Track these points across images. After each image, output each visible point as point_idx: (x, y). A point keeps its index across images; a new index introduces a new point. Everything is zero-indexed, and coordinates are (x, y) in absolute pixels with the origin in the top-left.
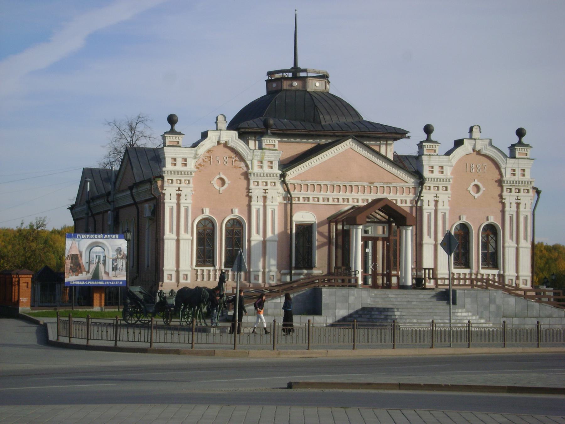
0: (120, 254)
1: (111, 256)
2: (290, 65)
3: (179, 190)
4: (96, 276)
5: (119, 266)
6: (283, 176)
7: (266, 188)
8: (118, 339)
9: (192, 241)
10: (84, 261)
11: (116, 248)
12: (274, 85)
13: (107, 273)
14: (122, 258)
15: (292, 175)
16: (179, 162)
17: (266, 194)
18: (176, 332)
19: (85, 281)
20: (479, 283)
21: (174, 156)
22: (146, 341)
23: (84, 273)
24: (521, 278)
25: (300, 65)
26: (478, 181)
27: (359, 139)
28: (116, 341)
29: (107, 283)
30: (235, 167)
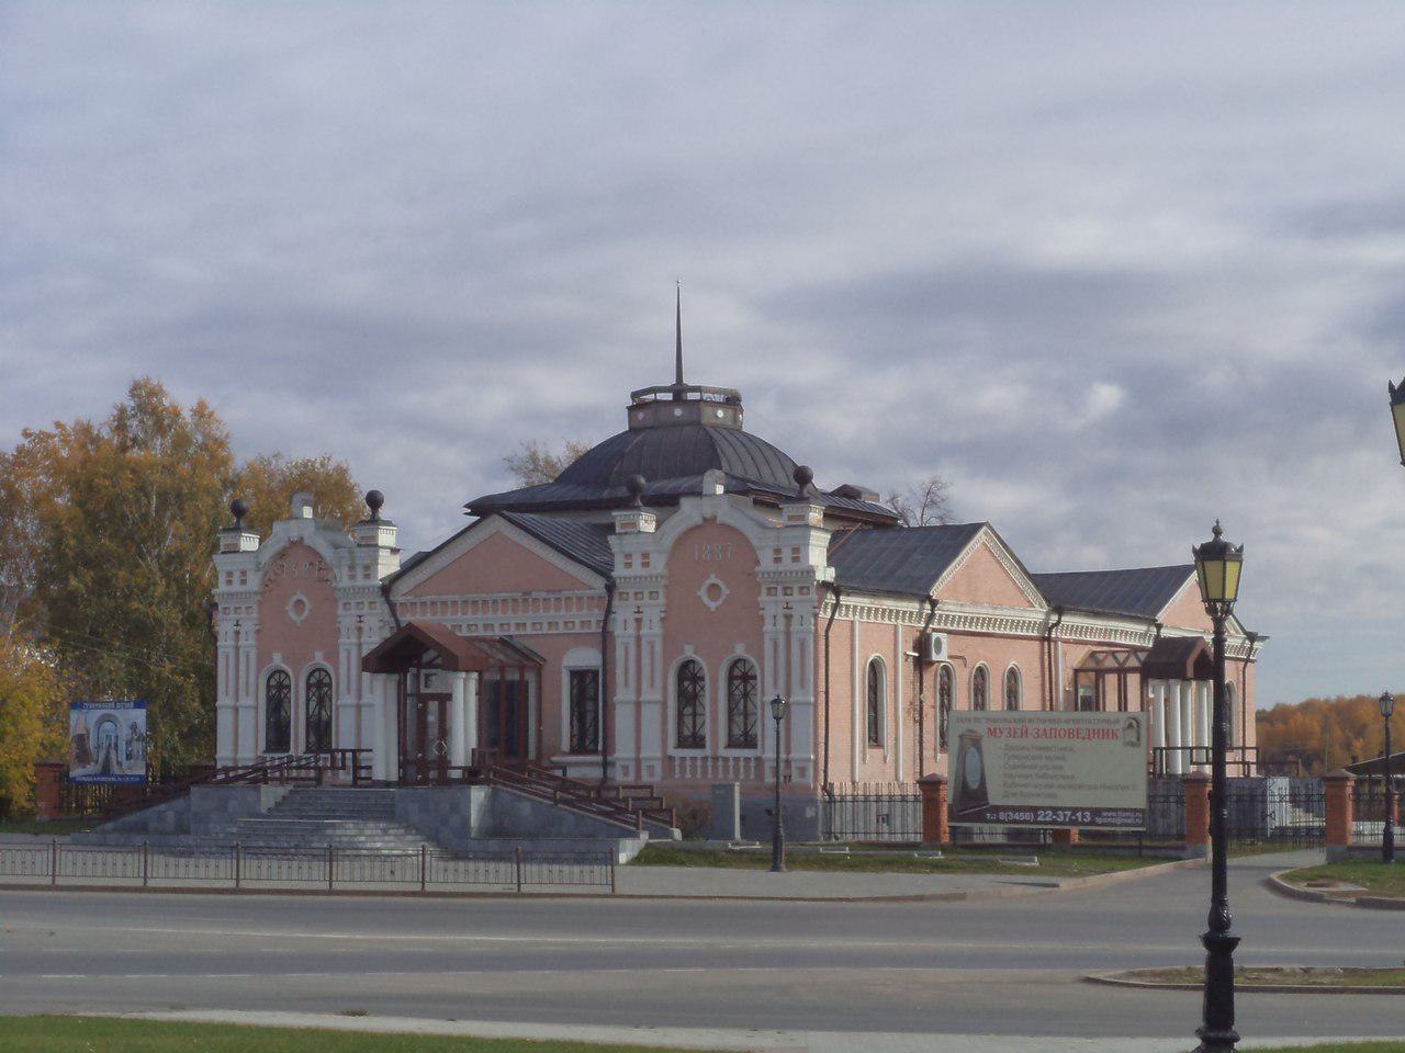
1: (124, 738)
2: (671, 380)
4: (106, 770)
7: (359, 613)
8: (149, 875)
9: (664, 704)
10: (92, 744)
12: (641, 416)
16: (236, 578)
17: (362, 625)
20: (277, 774)
21: (229, 568)
22: (509, 881)
24: (794, 765)
25: (688, 381)
26: (717, 577)
27: (514, 515)
28: (331, 881)
29: (120, 779)
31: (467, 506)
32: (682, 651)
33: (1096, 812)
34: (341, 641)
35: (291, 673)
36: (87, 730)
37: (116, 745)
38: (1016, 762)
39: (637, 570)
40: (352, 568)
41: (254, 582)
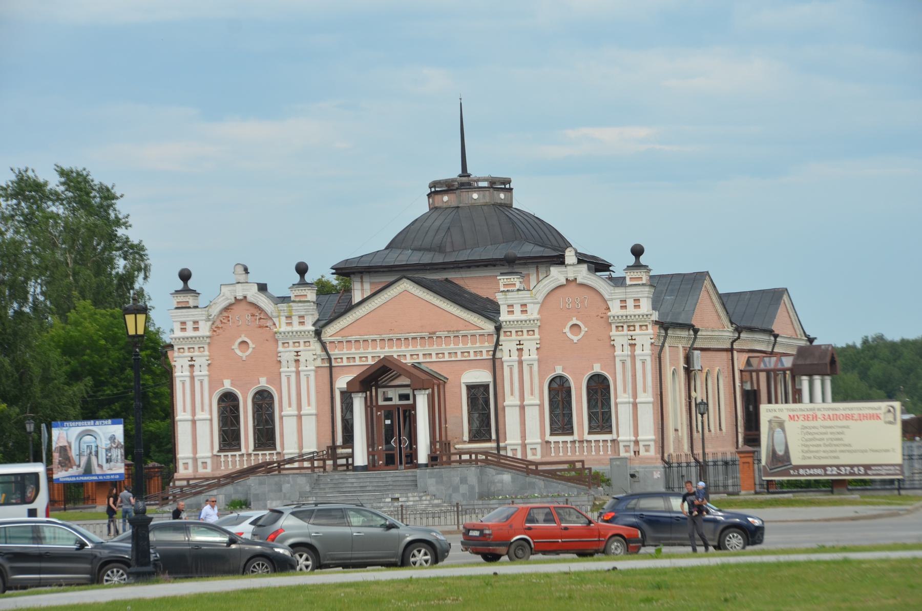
0: (114, 442)
1: (104, 446)
3: (192, 360)
4: (88, 471)
5: (114, 457)
6: (318, 333)
7: (297, 349)
10: (74, 453)
11: (109, 435)
13: (100, 466)
14: (117, 447)
15: (329, 333)
19: (75, 476)
23: (75, 467)
29: (101, 478)
30: (260, 327)
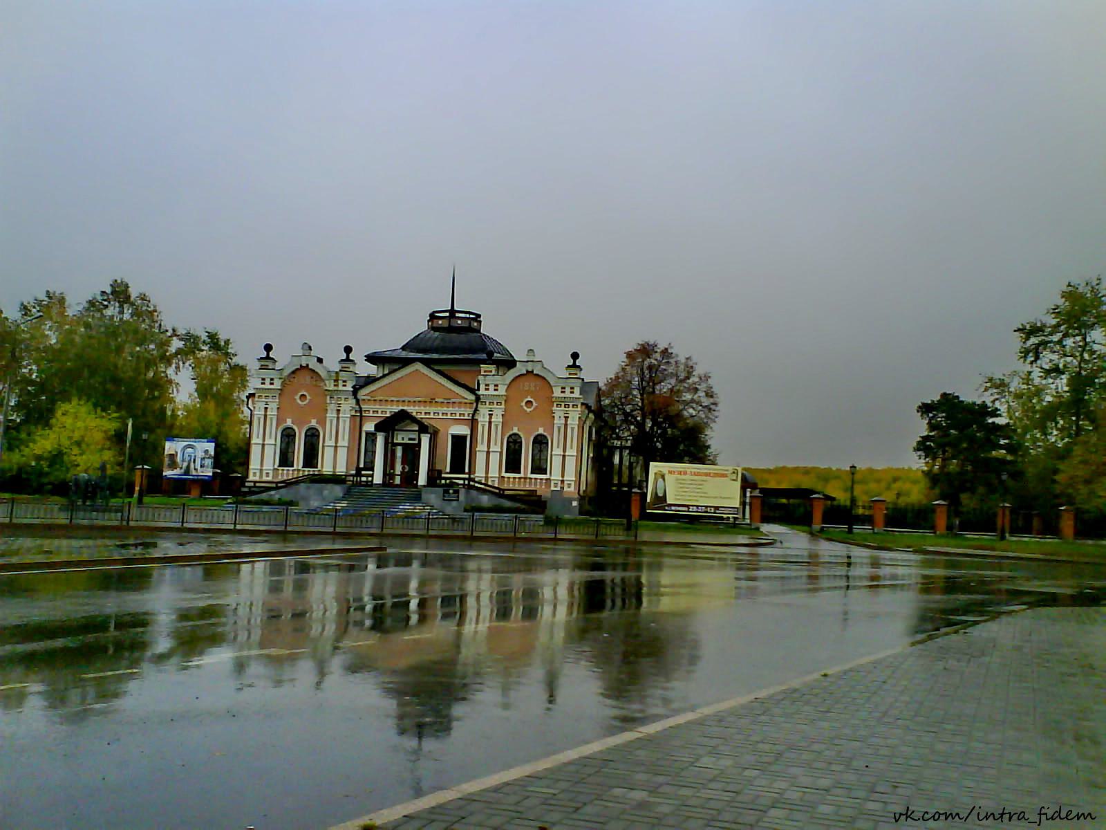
1: (200, 456)
4: (187, 472)
8: (185, 521)
9: (501, 453)
10: (179, 459)
18: (608, 527)
23: (178, 469)
28: (183, 522)
31: (366, 356)
32: (310, 422)
33: (717, 508)
34: (328, 415)
35: (522, 436)
36: (177, 453)
37: (194, 460)
38: (681, 486)
39: (491, 392)
40: (336, 381)
41: (277, 384)
